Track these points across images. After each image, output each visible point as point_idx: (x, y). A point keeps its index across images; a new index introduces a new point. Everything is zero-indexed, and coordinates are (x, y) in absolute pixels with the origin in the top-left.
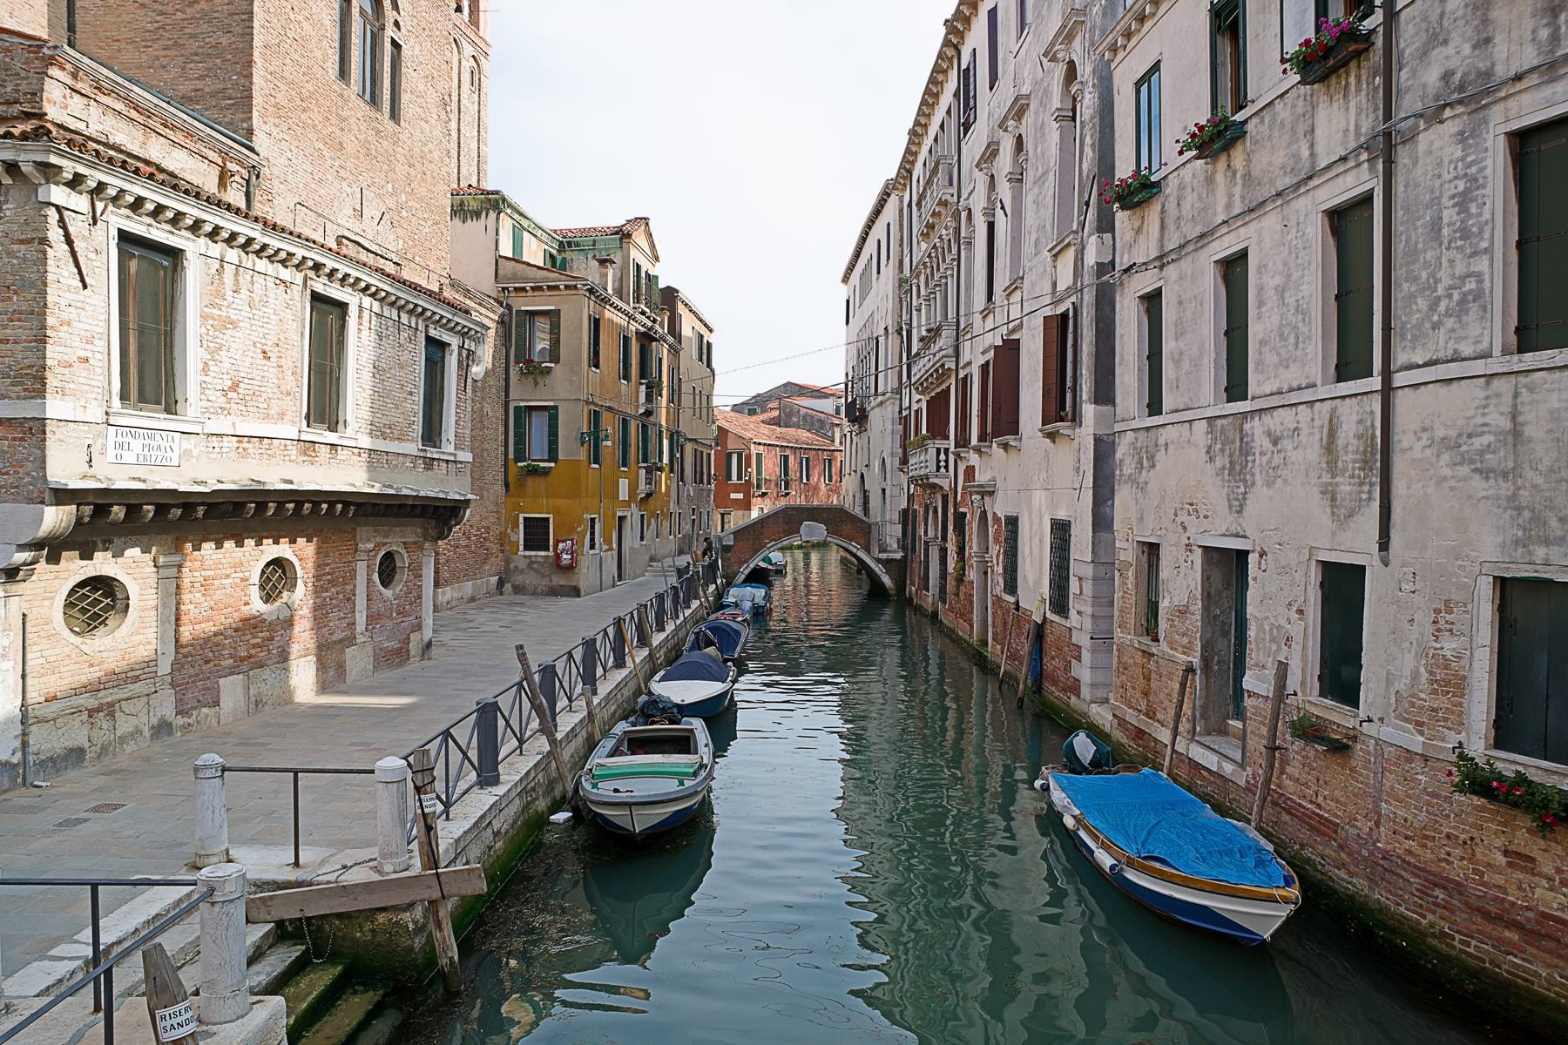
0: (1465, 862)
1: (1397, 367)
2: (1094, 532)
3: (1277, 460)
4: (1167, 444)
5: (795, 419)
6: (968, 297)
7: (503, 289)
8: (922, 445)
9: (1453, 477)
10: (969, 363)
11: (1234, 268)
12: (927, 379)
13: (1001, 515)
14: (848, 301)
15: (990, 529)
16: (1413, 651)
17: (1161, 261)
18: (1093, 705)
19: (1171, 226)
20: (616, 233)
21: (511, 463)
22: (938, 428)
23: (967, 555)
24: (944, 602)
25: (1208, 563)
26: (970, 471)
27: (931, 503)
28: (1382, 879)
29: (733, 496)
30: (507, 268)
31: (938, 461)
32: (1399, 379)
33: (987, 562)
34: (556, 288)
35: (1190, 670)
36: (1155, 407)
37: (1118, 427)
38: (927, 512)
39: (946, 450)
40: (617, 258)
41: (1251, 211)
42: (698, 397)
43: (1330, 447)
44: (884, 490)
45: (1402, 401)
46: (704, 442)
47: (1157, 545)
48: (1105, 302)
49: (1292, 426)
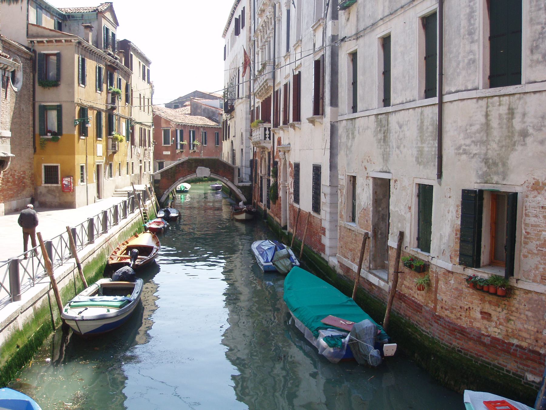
0: (467, 318)
1: (445, 93)
2: (330, 170)
3: (401, 136)
4: (359, 127)
5: (199, 111)
6: (279, 49)
7: (31, 42)
8: (257, 126)
9: (464, 144)
10: (280, 83)
11: (386, 42)
12: (260, 91)
13: (292, 162)
14: (225, 48)
15: (288, 169)
16: (449, 224)
17: (357, 36)
18: (330, 257)
19: (361, 20)
20: (95, 11)
22: (266, 119)
23: (278, 183)
24: (269, 208)
25: (375, 185)
27: (263, 156)
28: (437, 329)
29: (165, 153)
30: (33, 30)
31: (265, 135)
32: (446, 98)
33: (286, 187)
34: (60, 41)
35: (366, 236)
36: (354, 109)
37: (340, 118)
38: (261, 161)
39: (269, 128)
40: (95, 25)
41: (391, 14)
42: (142, 100)
43: (421, 128)
44: (242, 149)
45: (447, 108)
46: (146, 124)
47: (356, 177)
48: (334, 55)
49: (407, 119)
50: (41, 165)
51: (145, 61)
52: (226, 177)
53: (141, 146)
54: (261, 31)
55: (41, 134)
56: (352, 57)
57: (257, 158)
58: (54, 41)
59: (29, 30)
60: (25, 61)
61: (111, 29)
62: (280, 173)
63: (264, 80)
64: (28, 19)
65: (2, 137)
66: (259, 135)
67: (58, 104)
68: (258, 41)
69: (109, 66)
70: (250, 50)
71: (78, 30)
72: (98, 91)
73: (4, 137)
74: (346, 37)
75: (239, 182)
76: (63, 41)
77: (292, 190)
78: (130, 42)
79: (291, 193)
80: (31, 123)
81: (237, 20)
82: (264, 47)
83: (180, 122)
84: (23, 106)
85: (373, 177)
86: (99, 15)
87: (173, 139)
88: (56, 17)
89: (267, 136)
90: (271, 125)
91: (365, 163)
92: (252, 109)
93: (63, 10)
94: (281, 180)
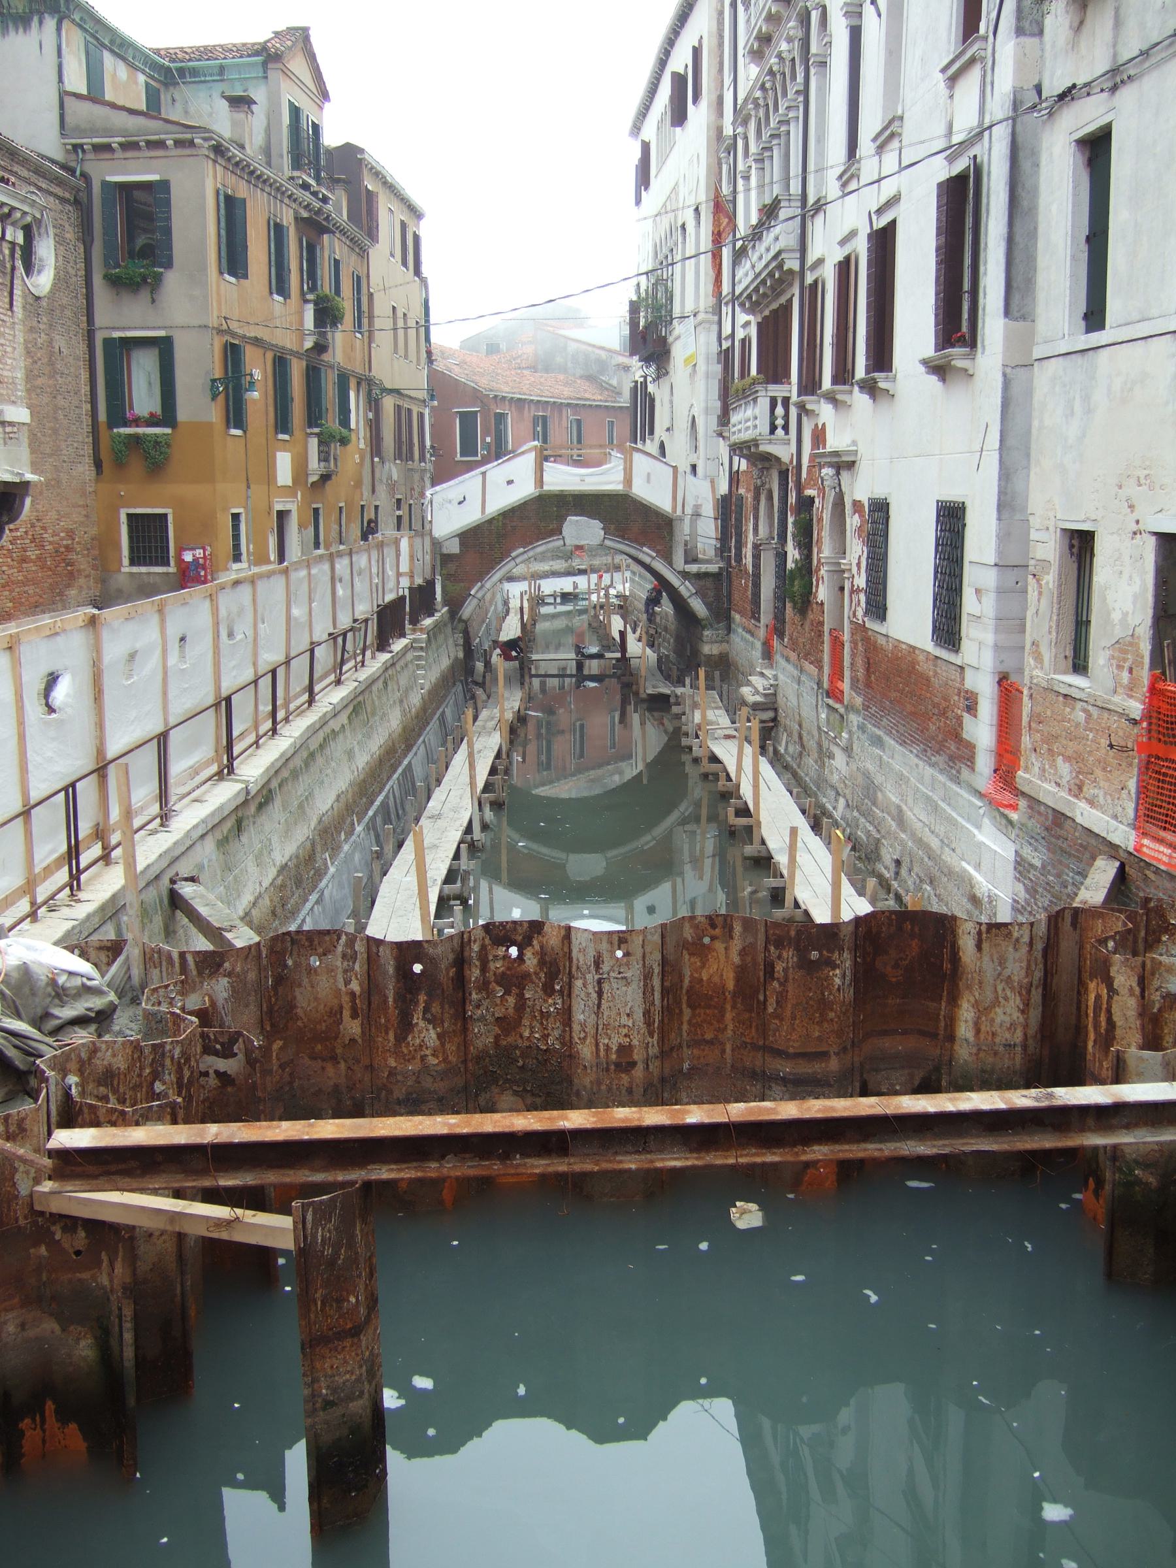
7: (75, 147)
10: (820, 262)
12: (756, 290)
15: (848, 520)
20: (257, 53)
21: (103, 428)
22: (775, 370)
26: (819, 436)
27: (763, 484)
30: (80, 111)
33: (843, 571)
36: (1094, 317)
38: (757, 498)
40: (259, 94)
46: (413, 394)
50: (119, 513)
51: (405, 209)
52: (649, 548)
53: (400, 458)
54: (757, 106)
55: (111, 424)
56: (1087, 154)
57: (742, 491)
58: (142, 144)
59: (68, 111)
60: (60, 207)
61: (309, 112)
62: (820, 530)
63: (772, 253)
64: (60, 80)
65: (3, 423)
66: (756, 418)
67: (162, 333)
68: (746, 138)
69: (303, 219)
70: (720, 168)
71: (210, 115)
72: (276, 297)
73: (11, 424)
74: (1074, 86)
75: (686, 562)
76: (170, 143)
77: (861, 581)
78: (362, 151)
79: (859, 590)
80: (85, 389)
81: (679, 81)
82: (766, 154)
83: (507, 389)
84: (60, 342)
85: (1155, 534)
86: (270, 66)
87: (488, 439)
88: (143, 72)
89: (780, 422)
90: (792, 389)
91: (1131, 490)
92: (725, 345)
93: (163, 53)
94: (825, 550)
